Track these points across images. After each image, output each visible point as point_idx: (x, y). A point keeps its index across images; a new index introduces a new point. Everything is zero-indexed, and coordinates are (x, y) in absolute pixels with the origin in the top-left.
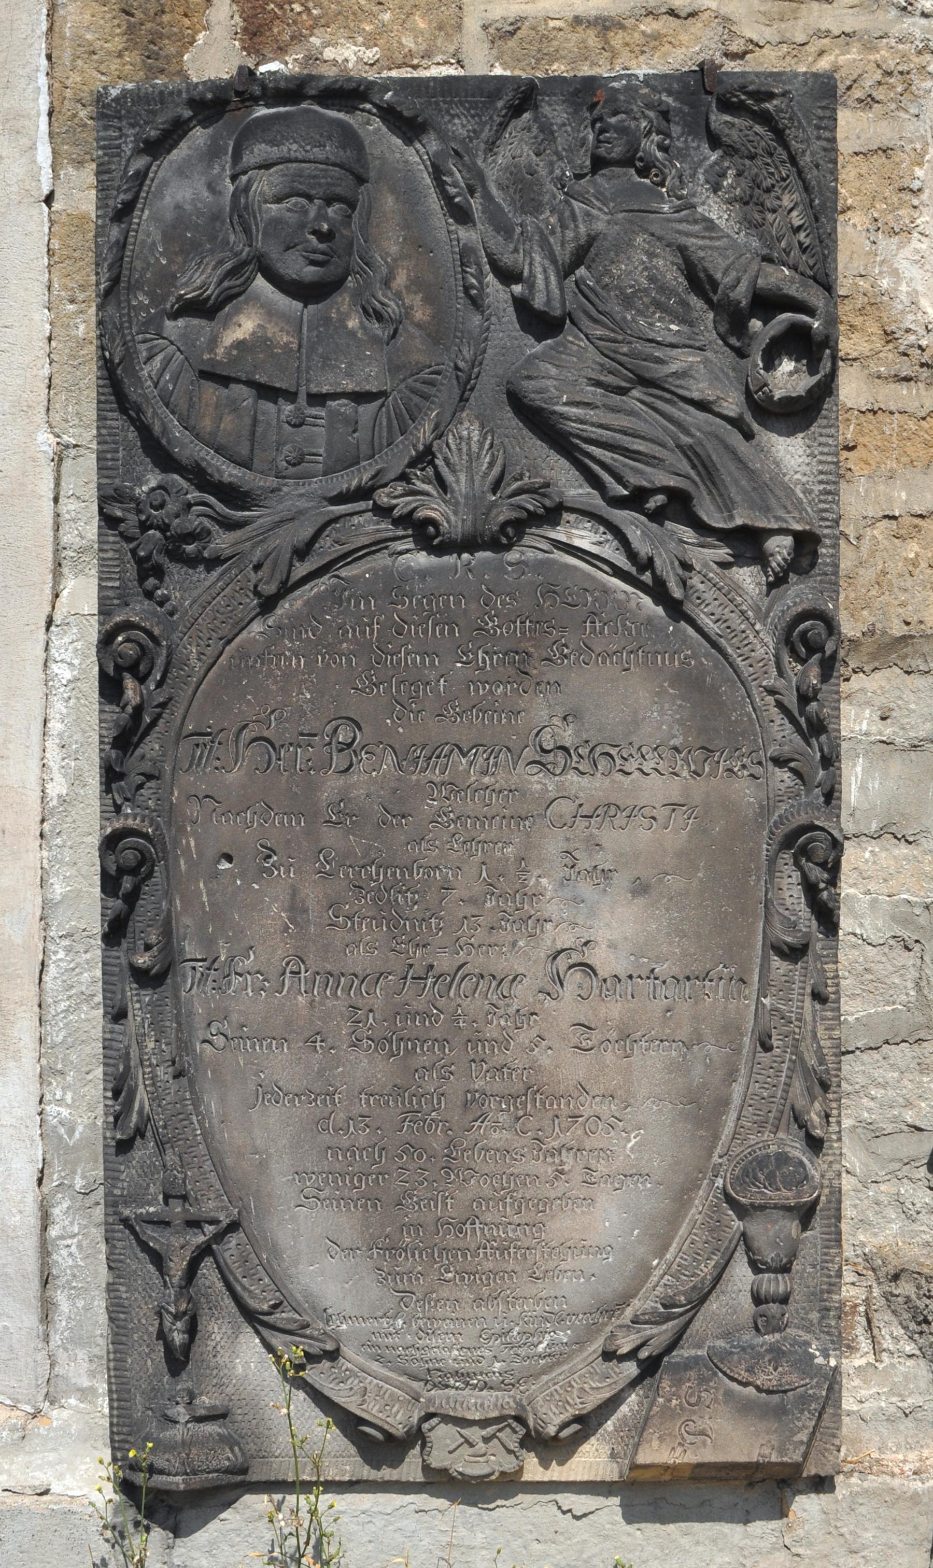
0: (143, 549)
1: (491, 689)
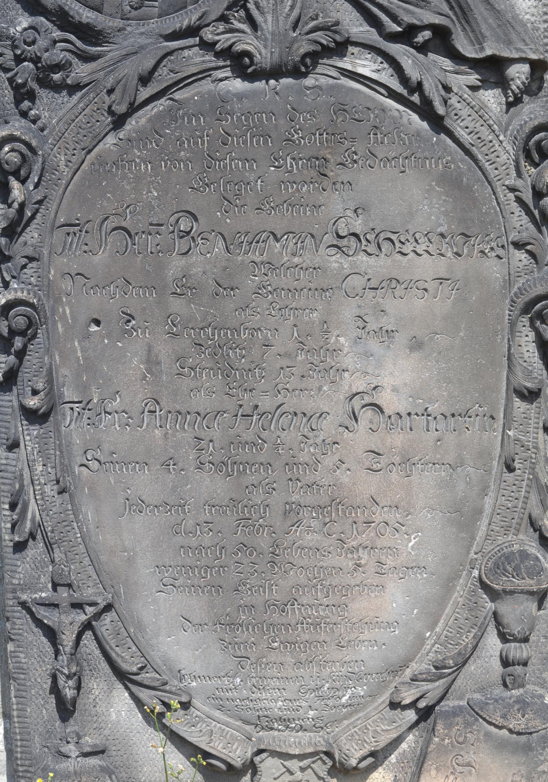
0: (20, 77)
1: (297, 188)
